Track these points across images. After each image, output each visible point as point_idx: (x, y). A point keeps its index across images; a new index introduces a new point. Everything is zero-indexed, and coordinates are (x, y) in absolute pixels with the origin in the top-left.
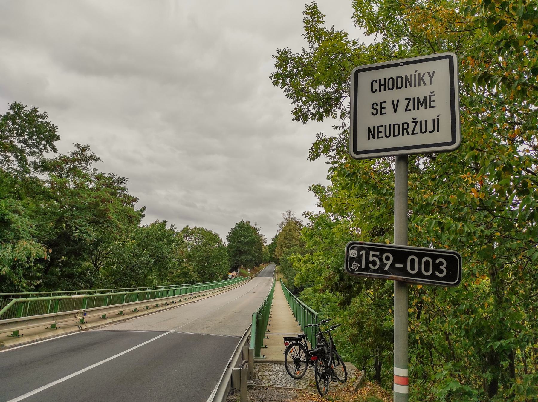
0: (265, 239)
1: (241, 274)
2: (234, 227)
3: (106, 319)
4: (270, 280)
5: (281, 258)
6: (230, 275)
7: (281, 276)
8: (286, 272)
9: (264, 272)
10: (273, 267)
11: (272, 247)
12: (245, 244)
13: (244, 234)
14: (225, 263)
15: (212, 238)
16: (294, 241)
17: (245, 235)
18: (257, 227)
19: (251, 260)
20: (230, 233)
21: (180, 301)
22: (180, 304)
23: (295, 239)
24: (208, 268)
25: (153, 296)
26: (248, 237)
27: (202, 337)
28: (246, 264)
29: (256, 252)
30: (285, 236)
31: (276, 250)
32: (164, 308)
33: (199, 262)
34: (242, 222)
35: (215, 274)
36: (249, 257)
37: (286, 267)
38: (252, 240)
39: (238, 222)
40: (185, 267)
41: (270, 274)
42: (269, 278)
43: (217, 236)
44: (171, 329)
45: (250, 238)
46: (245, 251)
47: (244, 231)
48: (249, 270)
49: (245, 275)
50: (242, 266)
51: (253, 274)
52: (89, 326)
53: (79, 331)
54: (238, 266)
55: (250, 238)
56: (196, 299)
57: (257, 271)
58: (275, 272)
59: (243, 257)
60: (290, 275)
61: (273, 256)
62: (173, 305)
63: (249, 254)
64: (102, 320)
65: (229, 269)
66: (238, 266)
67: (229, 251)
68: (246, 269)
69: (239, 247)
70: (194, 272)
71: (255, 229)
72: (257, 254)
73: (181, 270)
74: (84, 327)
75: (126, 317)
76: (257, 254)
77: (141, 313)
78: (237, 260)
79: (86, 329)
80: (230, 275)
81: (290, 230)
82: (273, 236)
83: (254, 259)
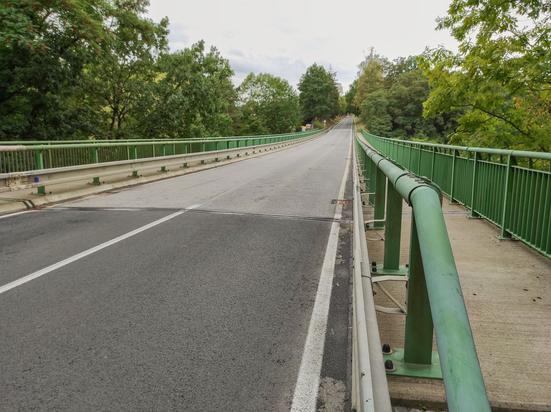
0: (341, 88)
1: (315, 127)
2: (305, 73)
3: (99, 184)
4: (349, 132)
5: (362, 104)
6: (304, 128)
7: (362, 127)
8: (368, 122)
9: (341, 124)
10: (352, 118)
11: (350, 97)
12: (319, 92)
13: (318, 83)
14: (297, 114)
15: (280, 86)
16: (378, 83)
17: (318, 82)
18: (332, 72)
19: (327, 111)
20: (301, 80)
21: (238, 155)
22: (238, 160)
23: (378, 81)
24: (279, 120)
25: (196, 148)
26: (322, 83)
27: (244, 223)
28: (321, 117)
29: (332, 101)
30: (367, 78)
31: (355, 97)
32: (213, 165)
33: (268, 114)
34: (315, 66)
35: (287, 127)
36: (324, 107)
37: (368, 114)
38: (327, 86)
39: (309, 66)
40: (254, 121)
41: (348, 125)
42: (347, 130)
43: (286, 83)
44: (193, 203)
45: (324, 84)
46: (319, 101)
47: (318, 76)
48: (325, 121)
49: (320, 128)
50: (316, 118)
51: (329, 127)
52: (55, 198)
53: (24, 210)
54: (312, 118)
55: (324, 84)
56: (261, 154)
57: (333, 123)
58: (354, 124)
59: (317, 108)
60: (374, 125)
61: (352, 105)
62: (228, 162)
63: (324, 104)
64: (68, 188)
65: (303, 121)
66: (312, 118)
67: (301, 102)
68: (321, 121)
69: (312, 96)
70: (264, 125)
71: (330, 75)
72: (333, 104)
73: (249, 124)
74: (39, 202)
75: (144, 180)
76: (333, 104)
77: (173, 174)
78: (310, 112)
79: (41, 207)
80: (304, 128)
81: (372, 71)
82: (351, 82)
83: (329, 109)
